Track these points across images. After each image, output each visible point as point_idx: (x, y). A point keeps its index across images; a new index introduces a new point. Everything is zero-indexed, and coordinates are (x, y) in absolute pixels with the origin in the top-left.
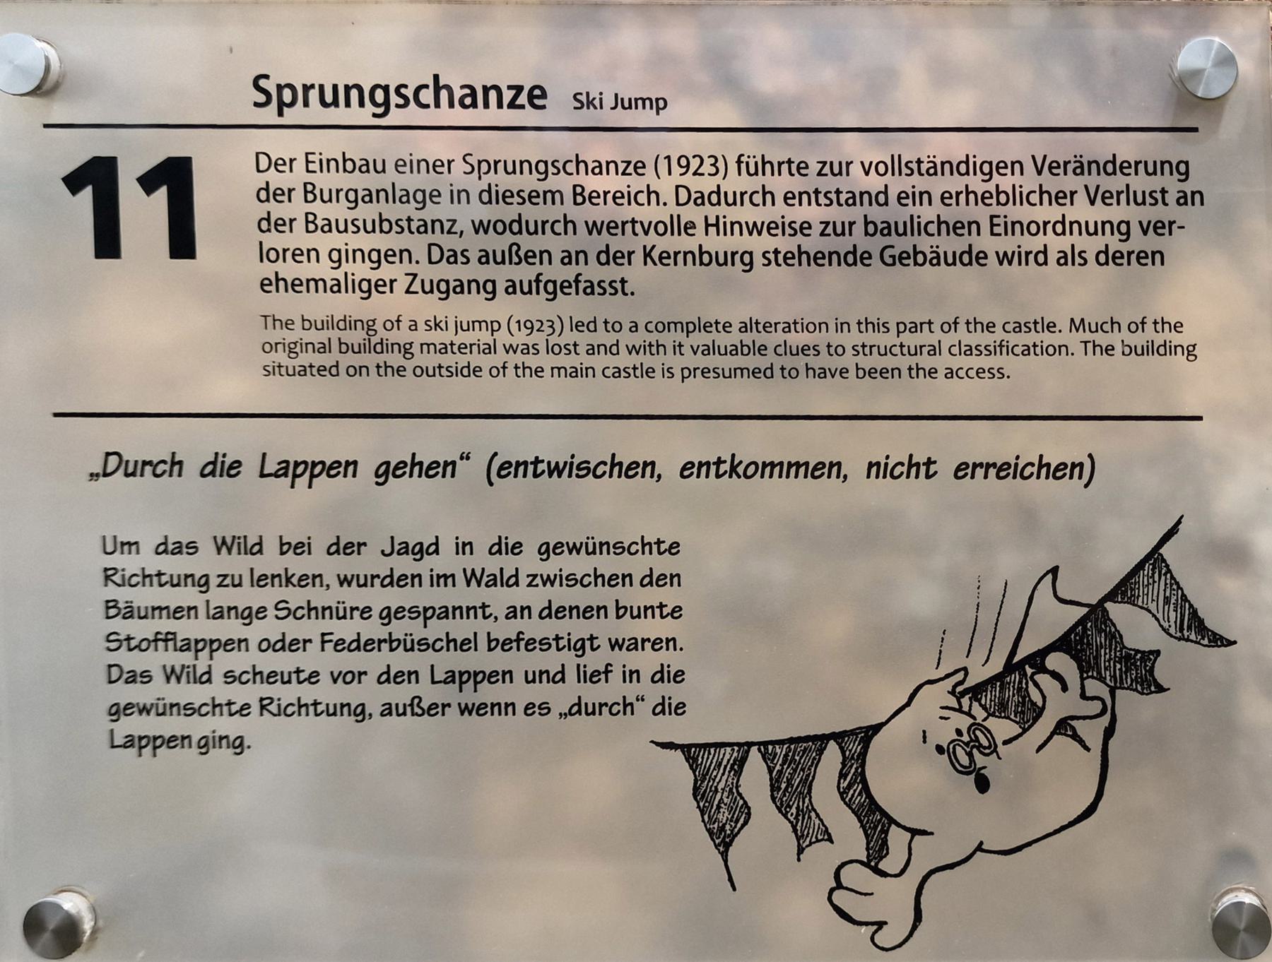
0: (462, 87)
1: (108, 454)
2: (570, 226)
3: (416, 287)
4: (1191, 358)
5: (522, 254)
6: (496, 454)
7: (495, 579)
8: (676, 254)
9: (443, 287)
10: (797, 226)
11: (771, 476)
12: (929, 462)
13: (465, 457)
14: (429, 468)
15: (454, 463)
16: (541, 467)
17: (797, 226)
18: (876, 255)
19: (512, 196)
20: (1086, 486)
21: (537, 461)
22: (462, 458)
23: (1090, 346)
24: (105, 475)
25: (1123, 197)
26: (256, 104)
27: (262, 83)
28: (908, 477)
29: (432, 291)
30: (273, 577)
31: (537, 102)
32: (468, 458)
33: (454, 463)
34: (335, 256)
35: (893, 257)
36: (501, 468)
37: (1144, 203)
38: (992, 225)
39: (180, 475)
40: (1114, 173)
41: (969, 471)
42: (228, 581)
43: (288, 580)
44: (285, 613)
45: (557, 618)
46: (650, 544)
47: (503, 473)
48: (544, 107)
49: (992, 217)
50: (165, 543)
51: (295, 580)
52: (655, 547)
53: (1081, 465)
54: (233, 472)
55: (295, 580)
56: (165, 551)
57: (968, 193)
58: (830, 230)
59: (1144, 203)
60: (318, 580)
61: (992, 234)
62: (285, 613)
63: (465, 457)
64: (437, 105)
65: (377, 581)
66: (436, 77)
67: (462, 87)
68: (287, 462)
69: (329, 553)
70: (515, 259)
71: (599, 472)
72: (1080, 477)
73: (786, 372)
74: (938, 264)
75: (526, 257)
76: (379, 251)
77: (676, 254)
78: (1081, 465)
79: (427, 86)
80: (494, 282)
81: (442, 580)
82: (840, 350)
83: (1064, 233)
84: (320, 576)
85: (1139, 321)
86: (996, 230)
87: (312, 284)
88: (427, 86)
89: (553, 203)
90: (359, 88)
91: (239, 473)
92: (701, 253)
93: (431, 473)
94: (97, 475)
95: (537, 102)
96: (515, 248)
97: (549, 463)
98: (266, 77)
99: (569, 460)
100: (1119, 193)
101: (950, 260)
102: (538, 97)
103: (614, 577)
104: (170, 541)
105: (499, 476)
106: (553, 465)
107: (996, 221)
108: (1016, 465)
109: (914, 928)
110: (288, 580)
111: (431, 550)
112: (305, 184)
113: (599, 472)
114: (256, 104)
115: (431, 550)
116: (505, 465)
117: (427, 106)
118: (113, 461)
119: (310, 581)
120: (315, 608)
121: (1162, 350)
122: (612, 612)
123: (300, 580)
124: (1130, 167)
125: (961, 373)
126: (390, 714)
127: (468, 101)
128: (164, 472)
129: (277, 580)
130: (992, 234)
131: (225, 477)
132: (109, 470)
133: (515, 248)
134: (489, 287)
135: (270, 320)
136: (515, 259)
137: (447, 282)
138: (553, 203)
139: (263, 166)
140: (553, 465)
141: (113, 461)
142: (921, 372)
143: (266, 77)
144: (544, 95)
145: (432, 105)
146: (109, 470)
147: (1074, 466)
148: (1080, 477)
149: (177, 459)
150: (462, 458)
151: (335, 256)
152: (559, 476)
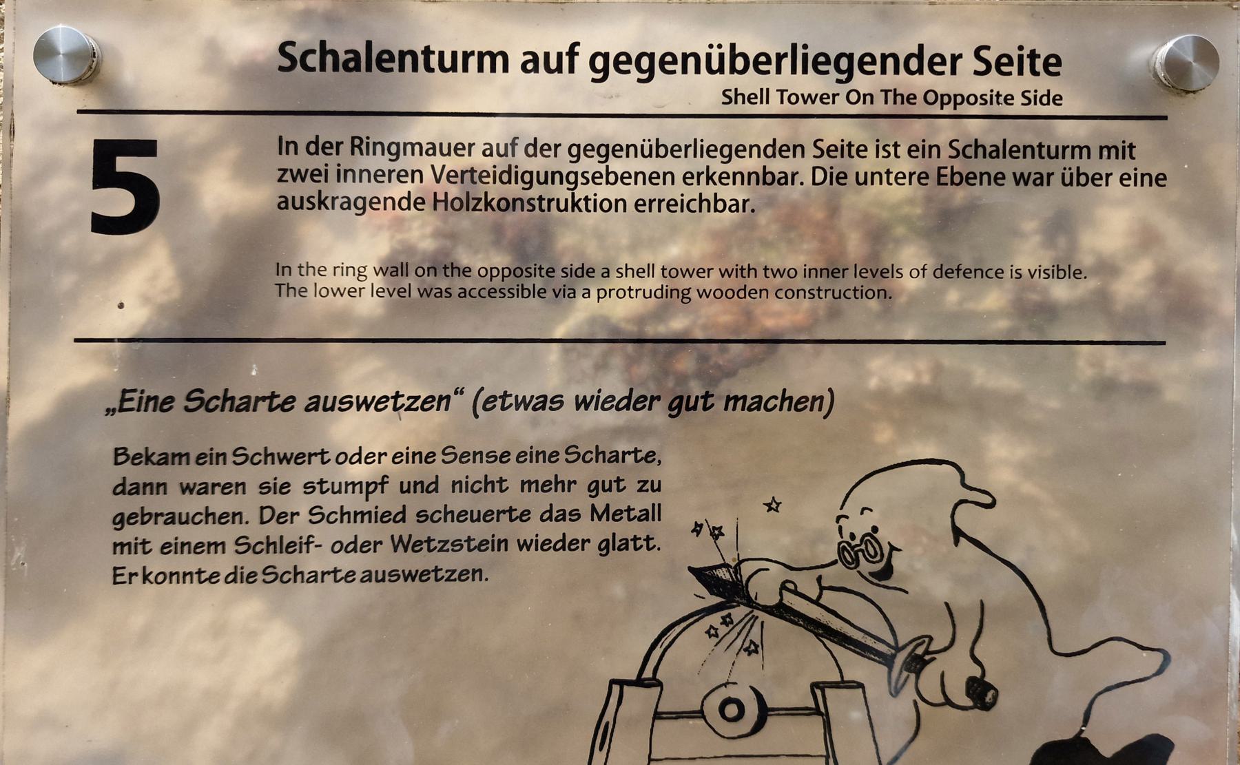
4: (686, 300)
6: (482, 389)
7: (647, 514)
8: (651, 202)
10: (589, 176)
11: (734, 409)
13: (459, 391)
14: (799, 402)
15: (448, 397)
16: (509, 401)
17: (589, 176)
20: (825, 417)
21: (505, 395)
22: (456, 393)
23: (284, 288)
24: (122, 410)
25: (691, 150)
26: (976, 73)
27: (983, 53)
28: (781, 409)
31: (1052, 69)
32: (462, 393)
33: (448, 397)
36: (487, 402)
37: (301, 207)
38: (940, 175)
39: (447, 409)
40: (409, 208)
41: (647, 403)
42: (648, 486)
44: (244, 548)
45: (570, 549)
46: (492, 482)
47: (488, 406)
48: (1058, 74)
49: (939, 168)
50: (123, 484)
52: (497, 486)
53: (821, 398)
54: (166, 407)
56: (123, 492)
60: (237, 518)
61: (939, 183)
62: (244, 548)
64: (323, 68)
67: (347, 52)
68: (318, 397)
69: (115, 493)
71: (211, 406)
72: (820, 409)
73: (666, 273)
74: (286, 208)
76: (364, 199)
77: (651, 202)
78: (821, 398)
79: (313, 52)
83: (509, 182)
84: (240, 513)
85: (955, 268)
86: (943, 180)
88: (313, 52)
89: (413, 154)
90: (895, 57)
91: (292, 407)
92: (716, 201)
93: (800, 407)
94: (114, 410)
95: (1052, 69)
97: (517, 397)
98: (988, 48)
99: (596, 394)
100: (687, 147)
101: (445, 151)
102: (669, 63)
103: (224, 515)
104: (128, 482)
105: (485, 409)
106: (520, 399)
107: (943, 172)
110: (148, 459)
111: (431, 488)
112: (353, 138)
113: (211, 406)
114: (976, 73)
115: (431, 488)
116: (491, 399)
117: (313, 69)
119: (230, 518)
124: (622, 150)
125: (474, 293)
127: (352, 65)
128: (217, 407)
130: (939, 183)
131: (158, 412)
138: (413, 154)
140: (520, 399)
143: (988, 48)
144: (1059, 63)
145: (318, 68)
147: (814, 399)
148: (820, 409)
149: (229, 395)
150: (456, 393)
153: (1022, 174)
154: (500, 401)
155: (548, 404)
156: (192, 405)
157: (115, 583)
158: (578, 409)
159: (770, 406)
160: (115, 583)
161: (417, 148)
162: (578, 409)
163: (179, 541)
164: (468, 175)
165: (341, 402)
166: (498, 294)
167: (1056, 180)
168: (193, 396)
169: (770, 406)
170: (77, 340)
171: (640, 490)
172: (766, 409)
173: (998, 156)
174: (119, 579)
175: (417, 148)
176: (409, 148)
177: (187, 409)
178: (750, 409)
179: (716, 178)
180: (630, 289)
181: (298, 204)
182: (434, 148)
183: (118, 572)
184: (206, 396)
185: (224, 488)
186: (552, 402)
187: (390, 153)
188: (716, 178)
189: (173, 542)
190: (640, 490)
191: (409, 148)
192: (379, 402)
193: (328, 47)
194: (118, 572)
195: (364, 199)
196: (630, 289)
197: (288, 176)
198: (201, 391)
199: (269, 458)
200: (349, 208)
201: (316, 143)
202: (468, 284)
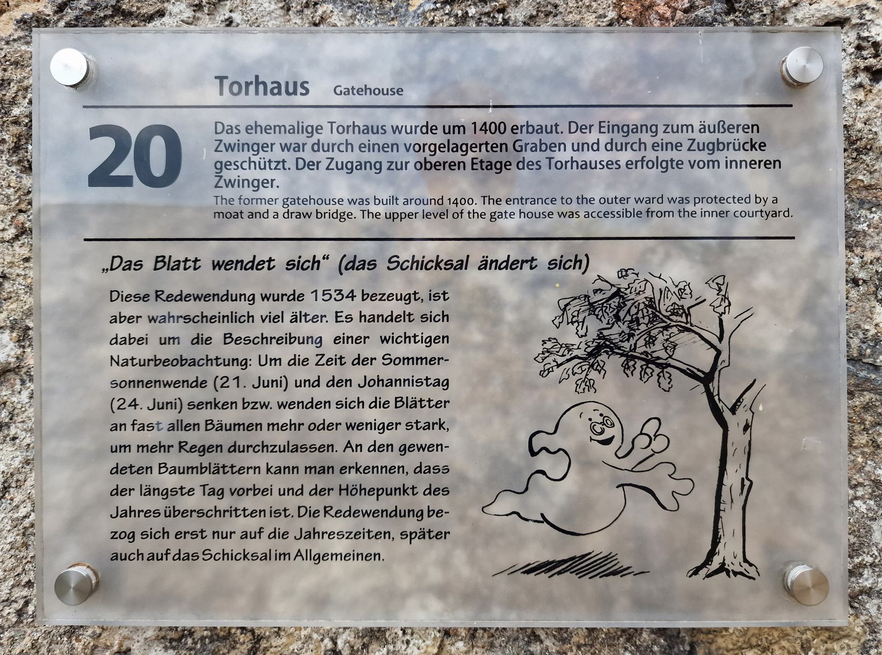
0: (272, 83)
1: (114, 257)
2: (643, 145)
3: (333, 166)
5: (726, 127)
6: (345, 256)
8: (760, 162)
9: (349, 165)
10: (395, 91)
12: (270, 260)
13: (326, 257)
18: (510, 146)
19: (231, 165)
20: (583, 273)
23: (366, 213)
24: (112, 269)
25: (639, 164)
28: (312, 269)
29: (342, 168)
30: (207, 403)
32: (328, 258)
34: (219, 165)
35: (521, 146)
37: (378, 132)
39: (318, 269)
41: (519, 265)
43: (216, 405)
51: (220, 405)
53: (581, 261)
54: (260, 267)
55: (220, 405)
57: (354, 126)
58: (669, 129)
59: (378, 132)
63: (326, 257)
65: (285, 298)
66: (257, 77)
67: (272, 83)
70: (722, 130)
72: (580, 268)
73: (564, 201)
75: (729, 128)
80: (380, 163)
81: (419, 361)
82: (569, 201)
87: (277, 128)
96: (722, 123)
107: (602, 124)
108: (299, 262)
109: (507, 515)
110: (216, 405)
113: (404, 267)
118: (117, 261)
120: (164, 446)
121: (396, 216)
122: (240, 405)
123: (223, 405)
125: (595, 215)
126: (153, 559)
127: (276, 91)
129: (209, 405)
132: (114, 267)
133: (722, 123)
134: (378, 166)
135: (487, 199)
136: (722, 130)
137: (628, 126)
139: (301, 166)
141: (117, 261)
142: (686, 214)
146: (114, 267)
148: (580, 268)
150: (324, 258)
151: (219, 165)
152: (220, 269)
153: (397, 127)
154: (267, 264)
155: (133, 266)
156: (552, 267)
157: (337, 321)
158: (214, 269)
159: (305, 266)
160: (337, 321)
161: (283, 128)
162: (214, 269)
163: (221, 315)
164: (483, 147)
165: (135, 265)
166: (610, 215)
167: (242, 129)
168: (393, 260)
169: (305, 266)
170: (85, 240)
171: (112, 538)
172: (565, 268)
173: (294, 132)
174: (339, 319)
175: (283, 128)
176: (685, 128)
177: (287, 269)
178: (172, 269)
179: (757, 146)
180: (506, 212)
181: (593, 166)
182: (368, 129)
183: (339, 314)
184: (401, 261)
185: (278, 340)
186: (369, 264)
187: (308, 132)
188: (757, 146)
189: (217, 315)
190: (112, 538)
191: (456, 129)
192: (227, 264)
193: (260, 80)
194: (339, 314)
195: (501, 163)
196: (522, 199)
197: (222, 148)
198: (398, 257)
199: (407, 340)
200: (491, 169)
201: (427, 126)
202: (590, 208)
